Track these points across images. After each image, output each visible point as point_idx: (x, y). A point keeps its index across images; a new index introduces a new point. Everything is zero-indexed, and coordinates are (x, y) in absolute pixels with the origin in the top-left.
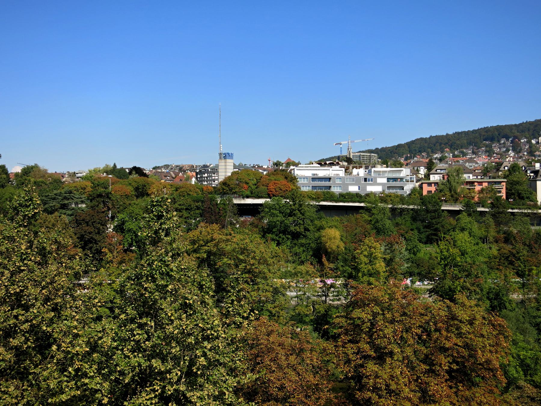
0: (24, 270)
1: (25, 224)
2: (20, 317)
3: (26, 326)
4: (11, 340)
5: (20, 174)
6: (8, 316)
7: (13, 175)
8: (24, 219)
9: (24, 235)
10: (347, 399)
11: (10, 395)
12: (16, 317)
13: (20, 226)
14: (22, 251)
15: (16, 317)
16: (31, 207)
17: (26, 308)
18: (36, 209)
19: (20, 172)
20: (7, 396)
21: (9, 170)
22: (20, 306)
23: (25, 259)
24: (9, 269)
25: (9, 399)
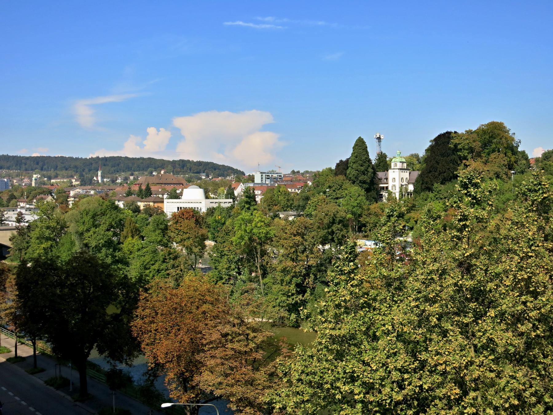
0: (532, 256)
1: (534, 209)
2: (528, 304)
3: (533, 314)
4: (519, 326)
5: (540, 159)
6: (516, 302)
7: (534, 160)
8: (533, 204)
9: (533, 220)
10: (460, 404)
11: (518, 380)
12: (524, 303)
13: (529, 211)
14: (529, 237)
15: (524, 303)
16: (541, 191)
17: (535, 295)
18: (545, 193)
19: (540, 156)
20: (515, 381)
21: (529, 156)
22: (528, 292)
23: (532, 245)
24: (519, 255)
25: (516, 385)
